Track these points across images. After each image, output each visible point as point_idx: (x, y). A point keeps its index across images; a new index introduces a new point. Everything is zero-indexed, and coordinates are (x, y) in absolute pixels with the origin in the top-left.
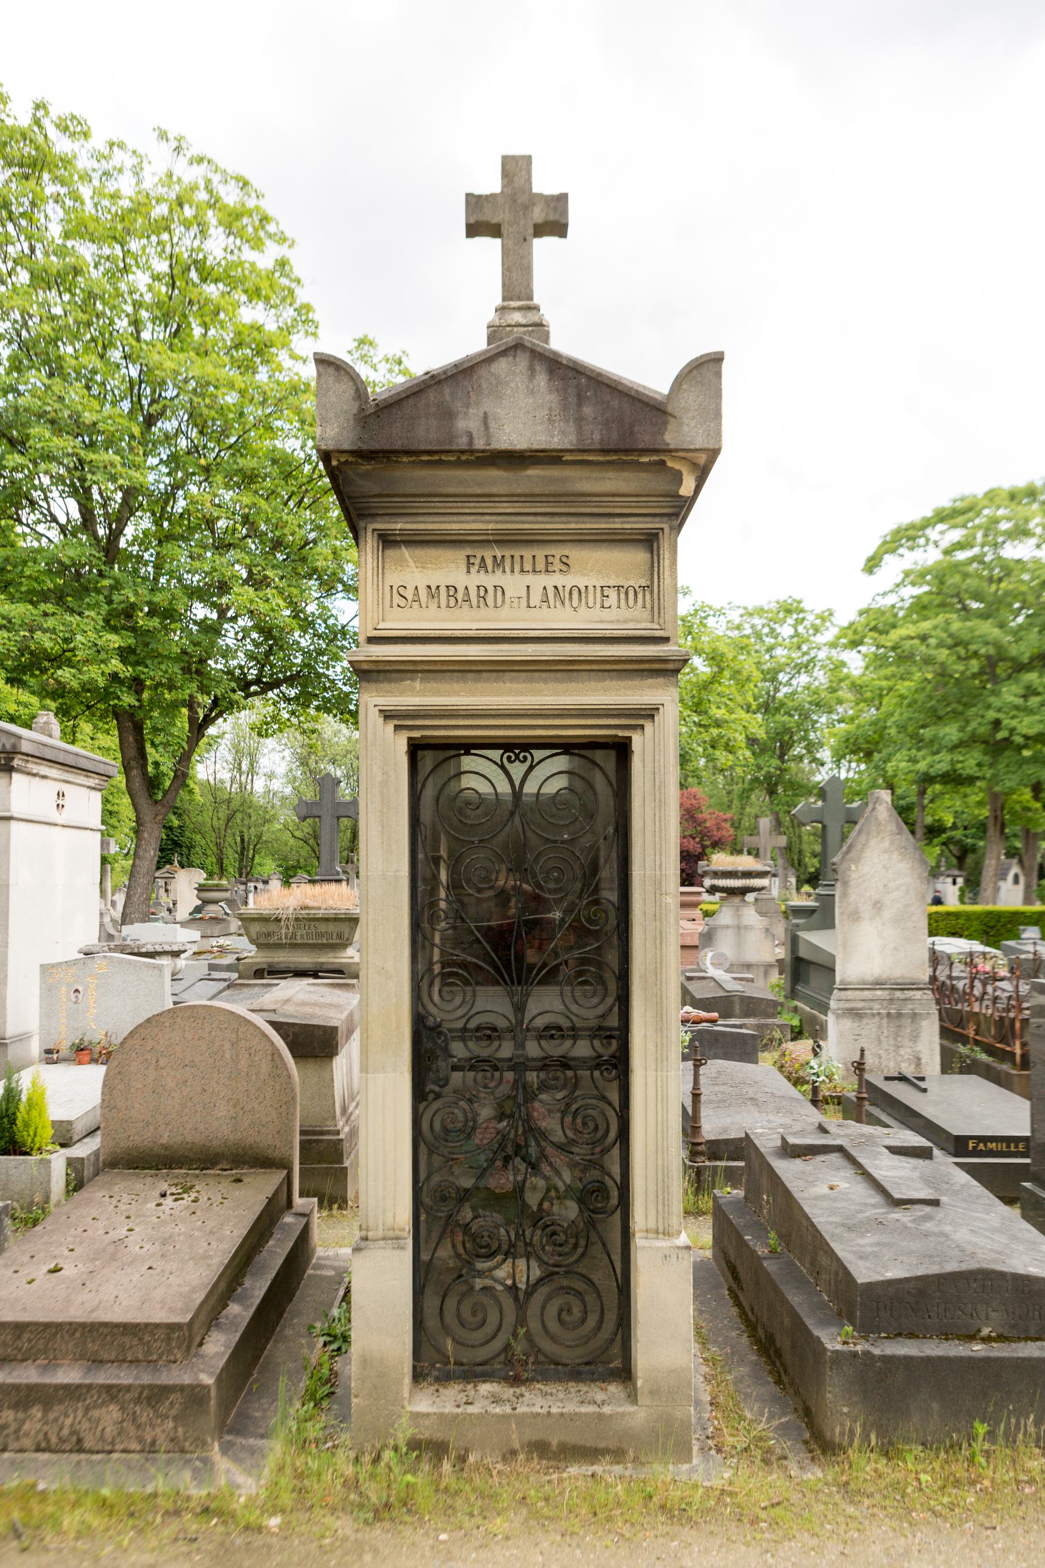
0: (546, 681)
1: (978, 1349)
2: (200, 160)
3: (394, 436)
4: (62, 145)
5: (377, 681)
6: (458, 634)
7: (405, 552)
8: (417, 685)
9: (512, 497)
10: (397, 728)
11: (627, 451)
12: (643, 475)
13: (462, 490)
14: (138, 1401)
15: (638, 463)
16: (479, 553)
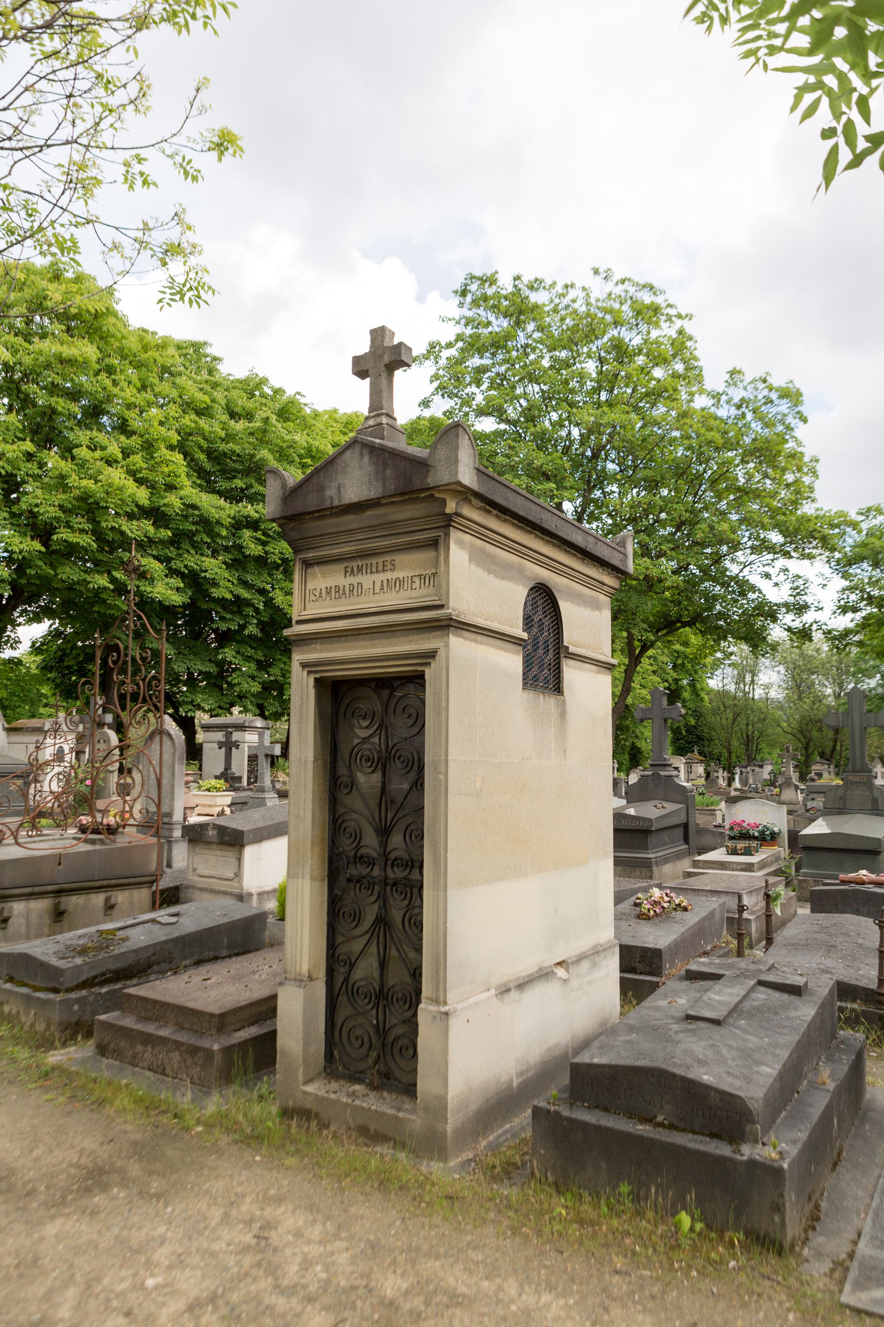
0: (379, 639)
1: (641, 1129)
2: (623, 282)
3: (299, 507)
4: (536, 298)
5: (300, 646)
6: (366, 611)
7: (317, 569)
8: (318, 647)
9: (361, 529)
10: (309, 672)
11: (412, 492)
12: (425, 504)
13: (336, 530)
14: (187, 1052)
15: (419, 498)
16: (350, 564)
